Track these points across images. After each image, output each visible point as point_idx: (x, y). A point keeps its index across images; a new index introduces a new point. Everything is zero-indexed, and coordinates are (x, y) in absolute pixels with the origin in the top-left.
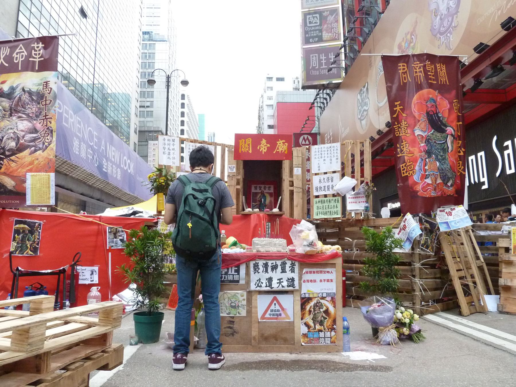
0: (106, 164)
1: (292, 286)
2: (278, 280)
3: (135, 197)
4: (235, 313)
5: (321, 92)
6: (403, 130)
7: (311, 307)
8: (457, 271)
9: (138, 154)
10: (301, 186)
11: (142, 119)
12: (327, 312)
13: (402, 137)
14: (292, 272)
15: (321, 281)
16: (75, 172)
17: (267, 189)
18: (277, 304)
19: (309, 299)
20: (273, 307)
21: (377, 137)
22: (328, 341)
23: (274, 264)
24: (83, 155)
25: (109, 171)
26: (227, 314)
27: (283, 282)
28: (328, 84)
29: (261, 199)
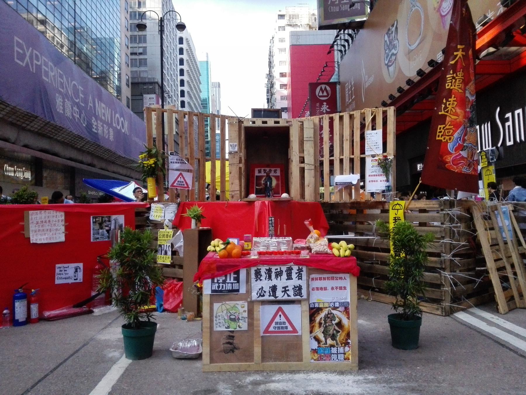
0: (95, 123)
1: (299, 295)
2: (283, 288)
4: (235, 327)
5: (342, 32)
6: (457, 82)
7: (321, 319)
8: (495, 261)
9: (132, 110)
10: (313, 163)
11: (135, 69)
12: (340, 324)
13: (453, 91)
14: (299, 279)
15: (332, 289)
17: (273, 172)
18: (282, 316)
20: (277, 319)
21: (406, 87)
22: (341, 357)
23: (279, 270)
24: (68, 114)
25: (100, 132)
26: (226, 328)
27: (288, 290)
28: (350, 23)
29: (266, 182)
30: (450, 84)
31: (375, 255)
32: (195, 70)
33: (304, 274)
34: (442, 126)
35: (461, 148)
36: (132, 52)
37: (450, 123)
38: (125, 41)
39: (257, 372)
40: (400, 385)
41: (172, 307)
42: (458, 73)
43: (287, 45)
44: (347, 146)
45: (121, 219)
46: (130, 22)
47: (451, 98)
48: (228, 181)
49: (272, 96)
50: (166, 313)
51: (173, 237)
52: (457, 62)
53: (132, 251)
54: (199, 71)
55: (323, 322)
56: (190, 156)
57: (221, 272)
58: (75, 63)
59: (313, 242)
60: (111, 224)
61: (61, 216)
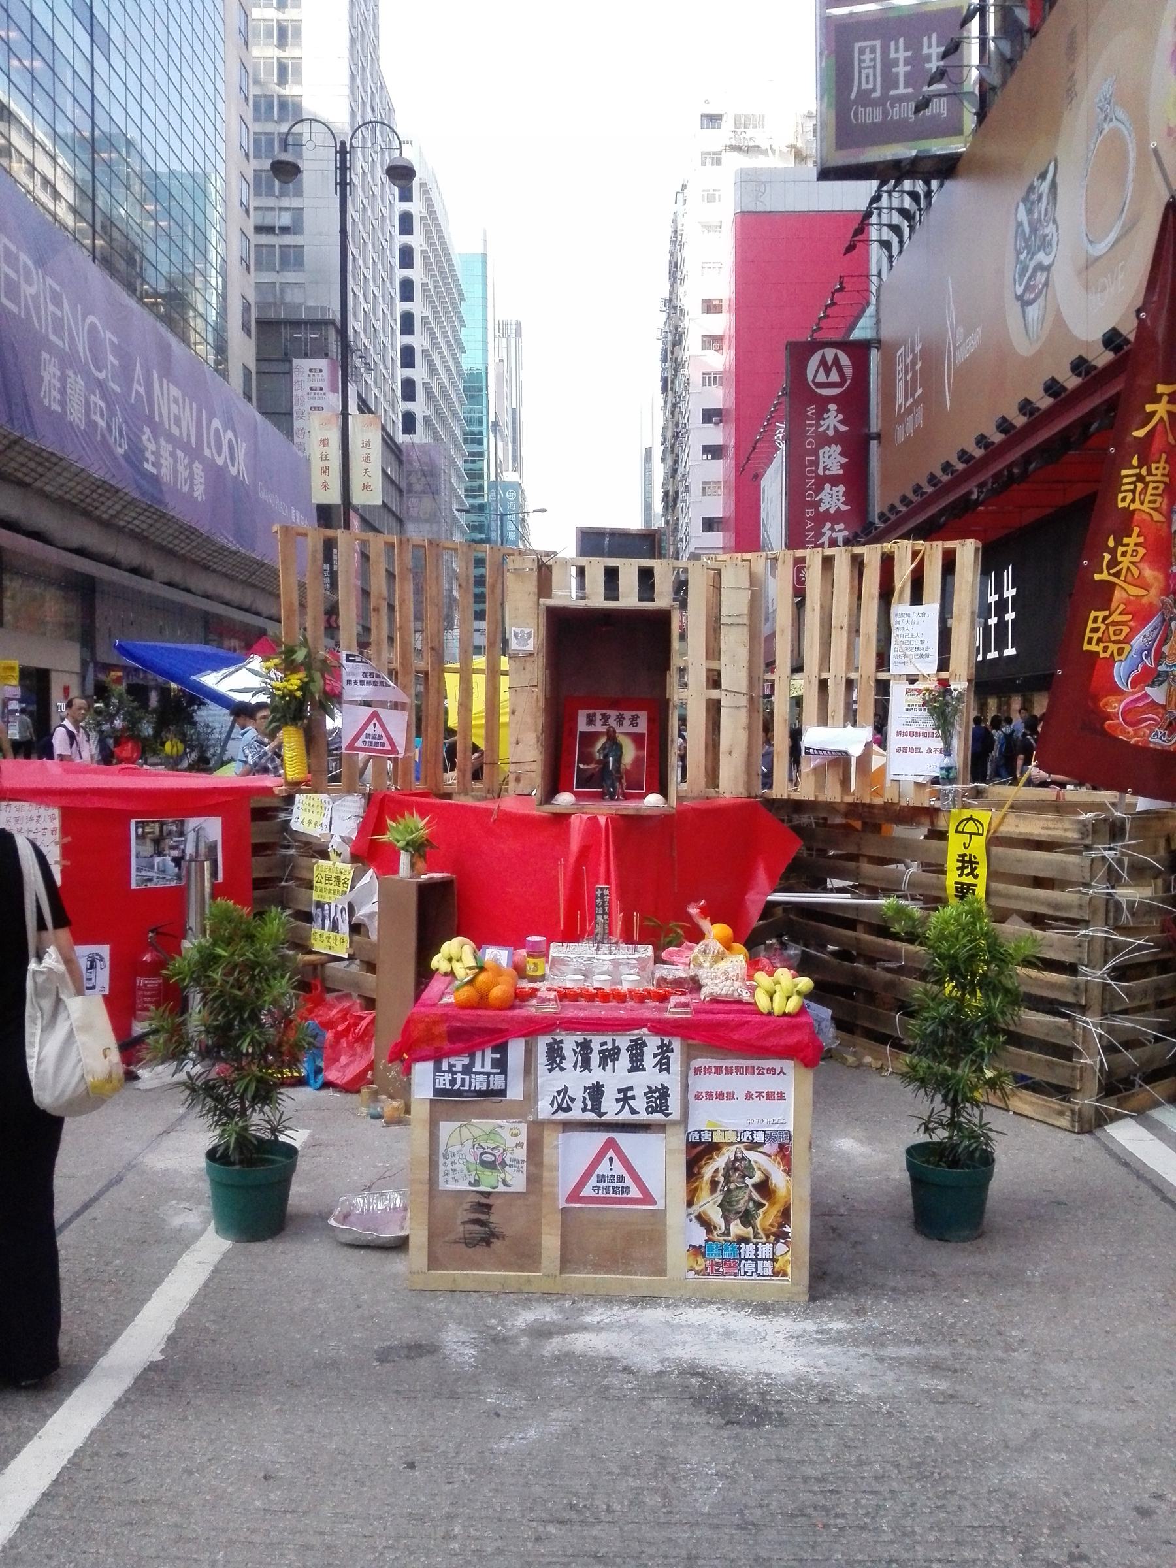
1: (661, 1111)
2: (620, 1091)
3: (257, 562)
6: (1150, 491)
7: (717, 1171)
10: (744, 687)
11: (268, 277)
12: (764, 1187)
14: (661, 1070)
15: (749, 1096)
16: (50, 475)
18: (616, 1160)
19: (713, 1148)
20: (603, 1168)
21: (1072, 382)
22: (766, 1268)
24: (76, 415)
25: (166, 473)
26: (471, 1184)
27: (633, 1098)
28: (915, 160)
29: (606, 756)
30: (1130, 496)
31: (907, 951)
32: (447, 284)
33: (675, 1058)
34: (1101, 614)
35: (1151, 677)
36: (259, 223)
37: (1122, 607)
38: (238, 191)
39: (547, 1297)
40: (906, 1351)
41: (346, 1079)
42: (1154, 466)
43: (726, 212)
44: (839, 641)
45: (213, 828)
46: (255, 127)
47: (1130, 536)
48: (506, 724)
49: (676, 370)
50: (330, 1092)
51: (352, 887)
52: (1151, 433)
53: (233, 969)
54: (458, 286)
55: (722, 1179)
56: (402, 664)
57: (460, 1045)
58: (94, 259)
59: (707, 964)
60: (185, 842)
61: (52, 818)
